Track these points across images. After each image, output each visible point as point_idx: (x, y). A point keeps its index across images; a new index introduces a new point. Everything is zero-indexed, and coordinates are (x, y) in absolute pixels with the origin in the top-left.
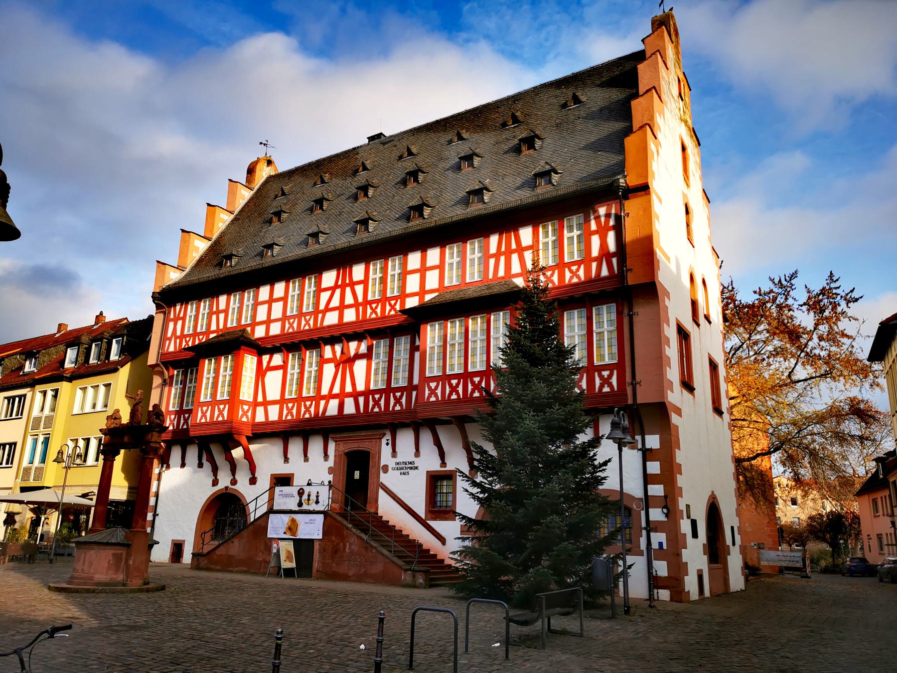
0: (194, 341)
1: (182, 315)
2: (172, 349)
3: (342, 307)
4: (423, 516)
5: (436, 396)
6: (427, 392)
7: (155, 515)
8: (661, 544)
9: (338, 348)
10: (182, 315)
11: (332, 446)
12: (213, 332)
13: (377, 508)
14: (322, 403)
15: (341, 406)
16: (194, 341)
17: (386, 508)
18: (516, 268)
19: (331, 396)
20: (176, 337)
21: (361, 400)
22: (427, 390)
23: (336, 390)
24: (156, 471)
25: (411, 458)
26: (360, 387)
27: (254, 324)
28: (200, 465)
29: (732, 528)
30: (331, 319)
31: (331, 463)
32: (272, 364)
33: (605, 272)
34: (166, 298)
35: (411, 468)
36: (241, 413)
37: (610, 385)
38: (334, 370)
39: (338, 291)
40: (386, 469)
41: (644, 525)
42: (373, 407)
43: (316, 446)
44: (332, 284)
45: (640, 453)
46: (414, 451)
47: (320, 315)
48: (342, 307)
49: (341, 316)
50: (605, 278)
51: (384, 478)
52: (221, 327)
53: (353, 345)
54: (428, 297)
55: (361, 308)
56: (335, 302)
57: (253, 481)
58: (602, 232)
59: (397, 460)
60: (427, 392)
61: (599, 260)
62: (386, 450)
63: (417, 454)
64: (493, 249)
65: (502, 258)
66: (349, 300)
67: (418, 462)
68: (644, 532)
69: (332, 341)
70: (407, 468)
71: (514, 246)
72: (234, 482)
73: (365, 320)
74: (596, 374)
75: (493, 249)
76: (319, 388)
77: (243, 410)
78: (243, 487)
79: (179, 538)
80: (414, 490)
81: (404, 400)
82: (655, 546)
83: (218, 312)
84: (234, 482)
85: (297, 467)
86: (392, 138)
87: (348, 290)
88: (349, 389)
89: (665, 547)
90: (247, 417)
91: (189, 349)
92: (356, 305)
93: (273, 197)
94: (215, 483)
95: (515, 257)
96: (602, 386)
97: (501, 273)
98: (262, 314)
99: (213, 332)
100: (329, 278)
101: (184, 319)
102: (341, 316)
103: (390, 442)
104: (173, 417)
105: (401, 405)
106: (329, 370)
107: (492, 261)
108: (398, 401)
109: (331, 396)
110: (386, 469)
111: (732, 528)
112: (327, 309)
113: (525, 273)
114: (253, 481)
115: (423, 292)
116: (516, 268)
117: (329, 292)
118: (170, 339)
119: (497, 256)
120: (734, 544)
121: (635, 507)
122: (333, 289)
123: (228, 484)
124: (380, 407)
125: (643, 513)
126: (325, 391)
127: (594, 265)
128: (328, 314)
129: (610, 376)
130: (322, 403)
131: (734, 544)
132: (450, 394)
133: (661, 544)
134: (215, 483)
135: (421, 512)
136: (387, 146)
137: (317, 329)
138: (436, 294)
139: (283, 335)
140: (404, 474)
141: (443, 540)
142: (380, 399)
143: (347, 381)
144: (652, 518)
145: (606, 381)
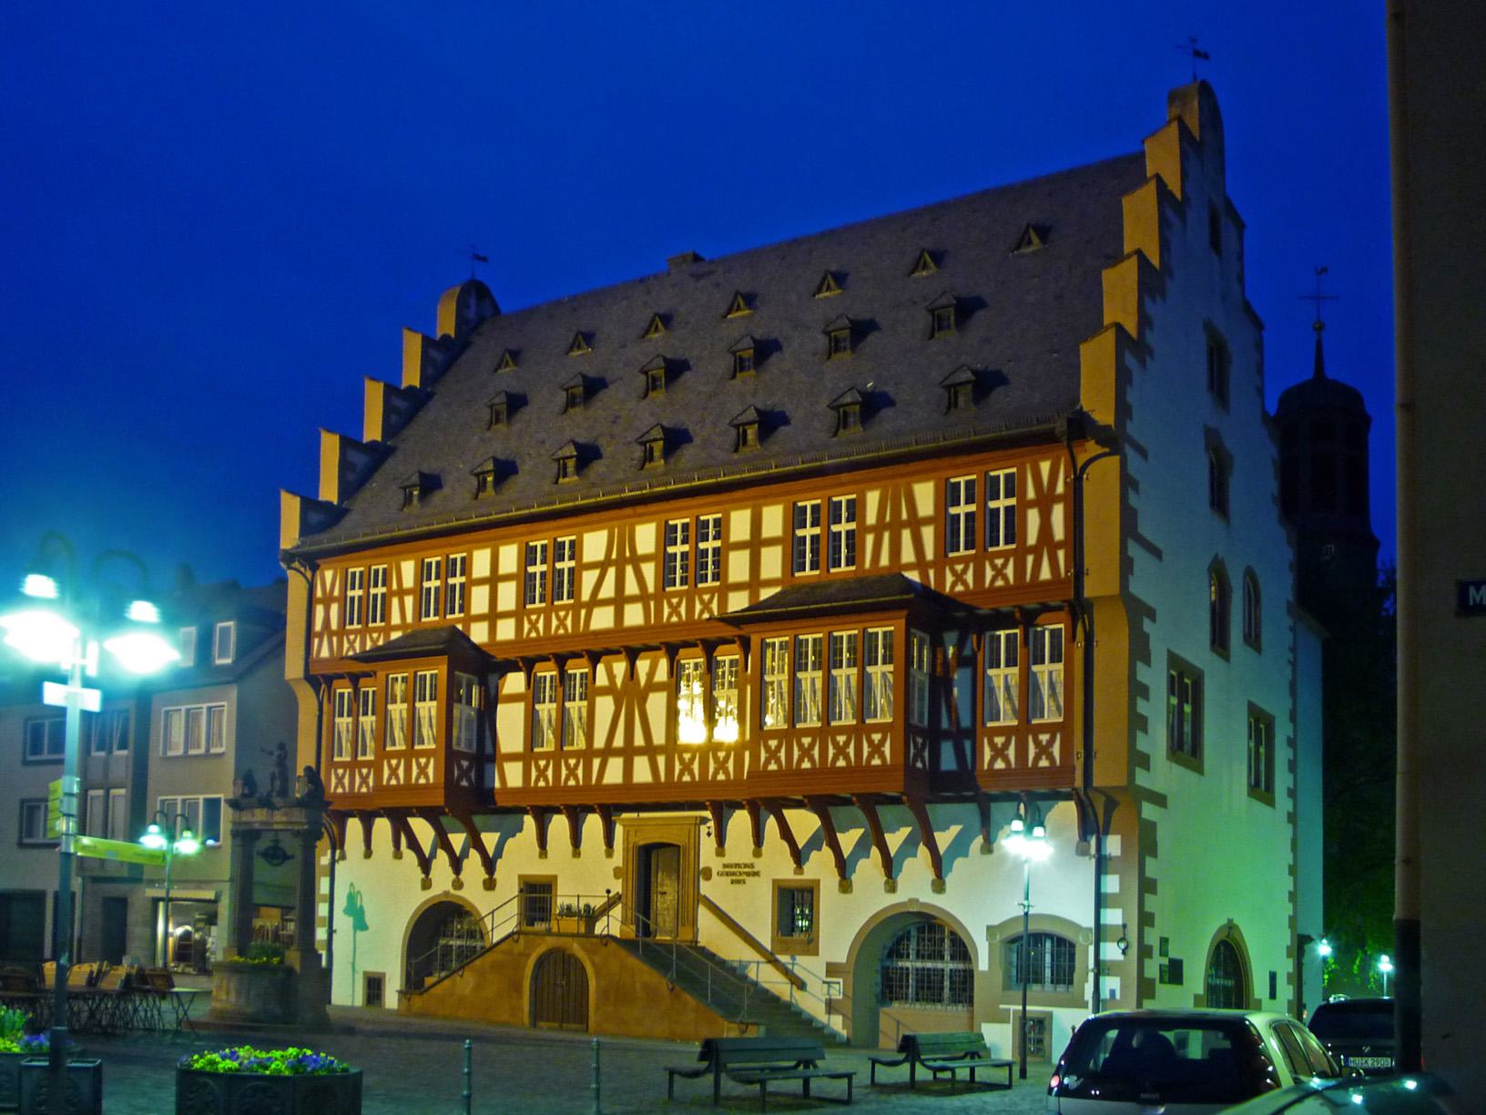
0: (363, 643)
2: (325, 653)
3: (619, 601)
5: (847, 757)
7: (331, 932)
8: (1113, 992)
12: (396, 628)
13: (696, 933)
14: (596, 762)
15: (628, 770)
16: (363, 643)
18: (908, 555)
19: (608, 752)
23: (619, 741)
24: (324, 860)
28: (398, 854)
29: (1273, 977)
30: (602, 619)
31: (618, 859)
33: (1045, 574)
35: (748, 874)
36: (887, 749)
37: (1051, 757)
38: (612, 707)
39: (611, 572)
40: (707, 874)
42: (567, 779)
46: (363, 848)
48: (619, 601)
49: (619, 615)
50: (1046, 583)
51: (705, 888)
52: (409, 619)
54: (766, 594)
56: (608, 590)
57: (490, 885)
58: (1045, 502)
59: (726, 860)
60: (887, 749)
61: (1036, 550)
62: (708, 844)
63: (757, 854)
65: (886, 536)
66: (631, 588)
67: (759, 864)
68: (1091, 976)
70: (739, 874)
72: (458, 884)
76: (589, 736)
78: (472, 892)
79: (374, 968)
82: (1105, 994)
84: (458, 884)
85: (557, 862)
87: (629, 570)
88: (639, 740)
89: (1118, 996)
90: (812, 759)
92: (643, 597)
94: (426, 884)
97: (885, 561)
102: (619, 615)
103: (713, 830)
104: (465, 764)
106: (605, 706)
109: (608, 752)
110: (707, 874)
111: (1273, 977)
112: (595, 602)
113: (921, 564)
114: (490, 885)
115: (755, 583)
116: (908, 555)
117: (597, 572)
118: (320, 635)
119: (878, 530)
120: (1273, 995)
122: (602, 566)
123: (449, 887)
124: (546, 780)
125: (1091, 949)
126: (599, 743)
128: (597, 612)
129: (1051, 742)
131: (1273, 995)
132: (801, 760)
133: (1113, 992)
134: (426, 884)
135: (765, 939)
137: (653, 627)
138: (777, 590)
139: (519, 641)
140: (738, 882)
141: (801, 986)
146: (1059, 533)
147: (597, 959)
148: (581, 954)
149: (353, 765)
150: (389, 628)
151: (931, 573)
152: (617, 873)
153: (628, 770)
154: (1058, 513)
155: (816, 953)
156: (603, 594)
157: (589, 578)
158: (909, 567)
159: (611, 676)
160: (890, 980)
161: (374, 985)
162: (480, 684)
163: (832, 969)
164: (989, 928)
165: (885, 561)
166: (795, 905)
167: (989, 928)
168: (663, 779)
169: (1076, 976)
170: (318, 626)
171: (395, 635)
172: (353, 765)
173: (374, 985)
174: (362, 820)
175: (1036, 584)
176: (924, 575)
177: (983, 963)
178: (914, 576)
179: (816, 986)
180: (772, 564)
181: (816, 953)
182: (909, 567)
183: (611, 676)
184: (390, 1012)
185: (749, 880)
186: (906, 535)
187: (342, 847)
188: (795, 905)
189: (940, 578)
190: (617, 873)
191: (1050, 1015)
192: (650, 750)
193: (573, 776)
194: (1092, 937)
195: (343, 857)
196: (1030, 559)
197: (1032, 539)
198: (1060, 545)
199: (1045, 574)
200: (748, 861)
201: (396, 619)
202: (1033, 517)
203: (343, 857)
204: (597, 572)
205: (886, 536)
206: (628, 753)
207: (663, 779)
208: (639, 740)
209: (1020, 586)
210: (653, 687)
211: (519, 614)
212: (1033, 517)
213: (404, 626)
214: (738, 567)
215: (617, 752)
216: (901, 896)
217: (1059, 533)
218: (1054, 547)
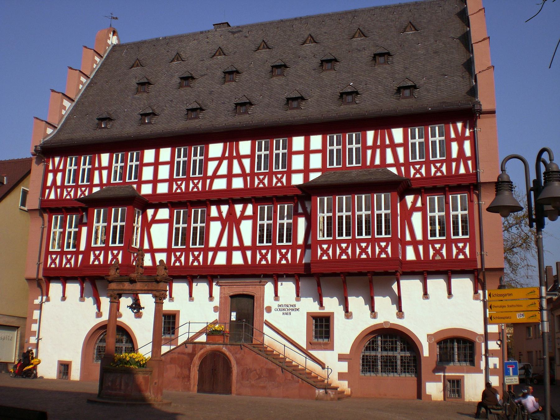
1: (61, 167)
2: (52, 197)
4: (304, 346)
6: (319, 252)
8: (495, 365)
9: (225, 209)
10: (61, 167)
11: (216, 289)
12: (96, 186)
14: (211, 254)
15: (229, 258)
17: (270, 338)
18: (390, 159)
20: (57, 187)
21: (249, 254)
22: (377, 248)
23: (224, 243)
25: (294, 302)
26: (419, 236)
27: (140, 183)
30: (220, 184)
31: (217, 302)
32: (158, 217)
33: (462, 171)
34: (46, 152)
40: (269, 309)
41: (483, 352)
43: (201, 288)
44: (219, 155)
45: (482, 302)
47: (208, 181)
51: (267, 316)
53: (238, 208)
54: (313, 176)
55: (248, 178)
56: (223, 170)
58: (460, 140)
61: (457, 160)
64: (370, 142)
65: (378, 151)
66: (236, 169)
67: (298, 305)
68: (484, 357)
69: (218, 203)
70: (287, 310)
71: (388, 142)
73: (252, 188)
74: (453, 245)
75: (370, 142)
77: (322, 249)
78: (127, 317)
79: (66, 359)
80: (297, 327)
81: (73, 261)
82: (491, 366)
83: (101, 169)
86: (239, 30)
88: (236, 243)
91: (80, 200)
93: (129, 64)
94: (99, 315)
95: (389, 151)
96: (458, 254)
97: (377, 162)
98: (147, 173)
99: (96, 186)
100: (216, 149)
101: (63, 171)
105: (70, 264)
106: (215, 228)
107: (369, 152)
108: (69, 261)
110: (269, 309)
112: (215, 176)
113: (397, 164)
115: (306, 170)
116: (390, 159)
117: (216, 163)
118: (50, 188)
119: (374, 148)
121: (477, 340)
122: (220, 160)
125: (483, 344)
126: (212, 243)
127: (454, 164)
130: (211, 254)
133: (495, 365)
134: (99, 315)
136: (236, 35)
142: (100, 255)
143: (232, 237)
144: (490, 348)
145: (461, 251)
146: (468, 153)
147: (238, 356)
148: (228, 353)
149: (62, 253)
150: (92, 186)
151: (403, 168)
152: (216, 309)
153: (229, 258)
154: (467, 145)
155: (332, 349)
156: (220, 173)
157: (212, 166)
158: (391, 165)
159: (220, 212)
160: (415, 366)
161: (65, 367)
162: (142, 214)
163: (341, 358)
164: (428, 335)
165: (377, 162)
166: (322, 327)
167: (428, 335)
168: (250, 262)
169: (476, 358)
170: (49, 184)
171: (95, 190)
172: (62, 253)
173: (65, 367)
174: (155, 296)
175: (457, 175)
176: (399, 170)
177: (426, 353)
178: (394, 170)
179: (333, 364)
180: (316, 161)
181: (332, 349)
182: (391, 165)
183: (220, 212)
184: (75, 382)
185: (292, 312)
186: (402, 160)
187: (47, 295)
188: (322, 327)
189: (408, 171)
190: (216, 309)
191: (463, 376)
192: (242, 248)
193: (196, 260)
194: (483, 339)
195: (48, 300)
196: (454, 164)
197: (454, 155)
198: (469, 158)
199: (462, 171)
200: (292, 304)
201: (96, 181)
202: (455, 146)
203: (48, 300)
204: (216, 163)
205: (378, 151)
206: (230, 249)
207: (250, 262)
208: (236, 243)
209: (449, 175)
210: (243, 217)
211: (170, 181)
212: (455, 146)
213: (101, 185)
214: (298, 162)
215: (223, 249)
216: (380, 320)
217: (468, 153)
218: (466, 159)
